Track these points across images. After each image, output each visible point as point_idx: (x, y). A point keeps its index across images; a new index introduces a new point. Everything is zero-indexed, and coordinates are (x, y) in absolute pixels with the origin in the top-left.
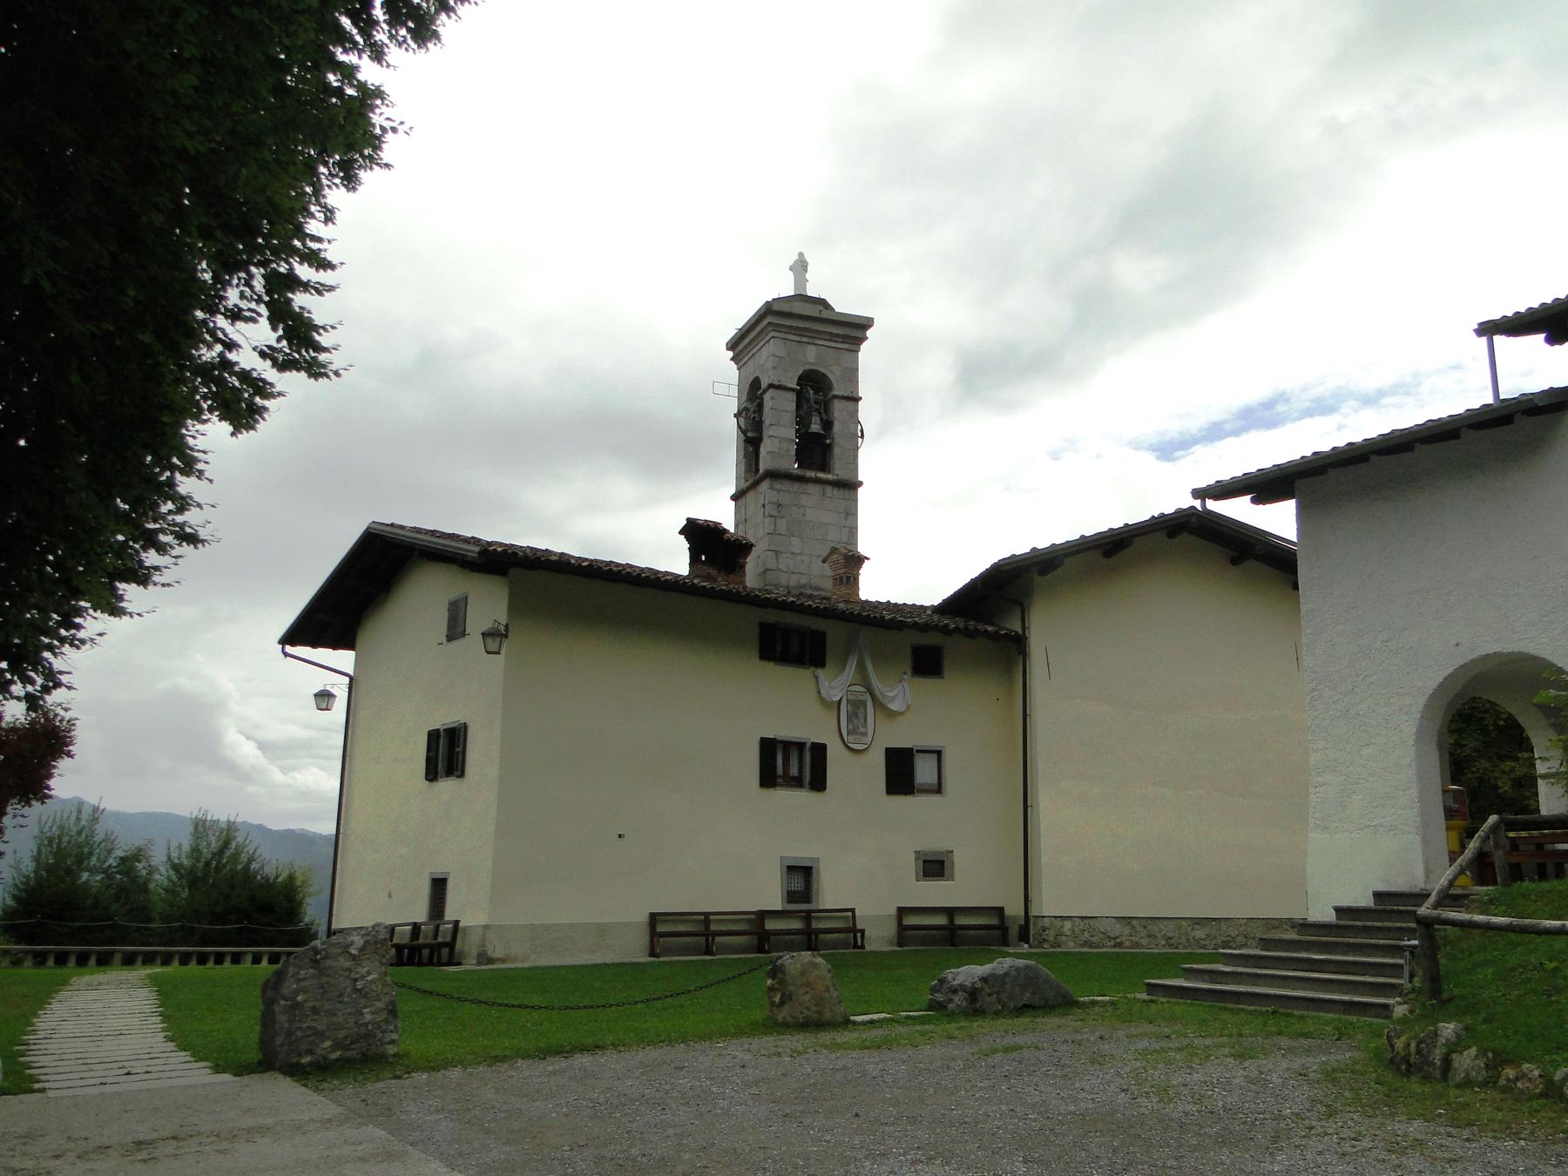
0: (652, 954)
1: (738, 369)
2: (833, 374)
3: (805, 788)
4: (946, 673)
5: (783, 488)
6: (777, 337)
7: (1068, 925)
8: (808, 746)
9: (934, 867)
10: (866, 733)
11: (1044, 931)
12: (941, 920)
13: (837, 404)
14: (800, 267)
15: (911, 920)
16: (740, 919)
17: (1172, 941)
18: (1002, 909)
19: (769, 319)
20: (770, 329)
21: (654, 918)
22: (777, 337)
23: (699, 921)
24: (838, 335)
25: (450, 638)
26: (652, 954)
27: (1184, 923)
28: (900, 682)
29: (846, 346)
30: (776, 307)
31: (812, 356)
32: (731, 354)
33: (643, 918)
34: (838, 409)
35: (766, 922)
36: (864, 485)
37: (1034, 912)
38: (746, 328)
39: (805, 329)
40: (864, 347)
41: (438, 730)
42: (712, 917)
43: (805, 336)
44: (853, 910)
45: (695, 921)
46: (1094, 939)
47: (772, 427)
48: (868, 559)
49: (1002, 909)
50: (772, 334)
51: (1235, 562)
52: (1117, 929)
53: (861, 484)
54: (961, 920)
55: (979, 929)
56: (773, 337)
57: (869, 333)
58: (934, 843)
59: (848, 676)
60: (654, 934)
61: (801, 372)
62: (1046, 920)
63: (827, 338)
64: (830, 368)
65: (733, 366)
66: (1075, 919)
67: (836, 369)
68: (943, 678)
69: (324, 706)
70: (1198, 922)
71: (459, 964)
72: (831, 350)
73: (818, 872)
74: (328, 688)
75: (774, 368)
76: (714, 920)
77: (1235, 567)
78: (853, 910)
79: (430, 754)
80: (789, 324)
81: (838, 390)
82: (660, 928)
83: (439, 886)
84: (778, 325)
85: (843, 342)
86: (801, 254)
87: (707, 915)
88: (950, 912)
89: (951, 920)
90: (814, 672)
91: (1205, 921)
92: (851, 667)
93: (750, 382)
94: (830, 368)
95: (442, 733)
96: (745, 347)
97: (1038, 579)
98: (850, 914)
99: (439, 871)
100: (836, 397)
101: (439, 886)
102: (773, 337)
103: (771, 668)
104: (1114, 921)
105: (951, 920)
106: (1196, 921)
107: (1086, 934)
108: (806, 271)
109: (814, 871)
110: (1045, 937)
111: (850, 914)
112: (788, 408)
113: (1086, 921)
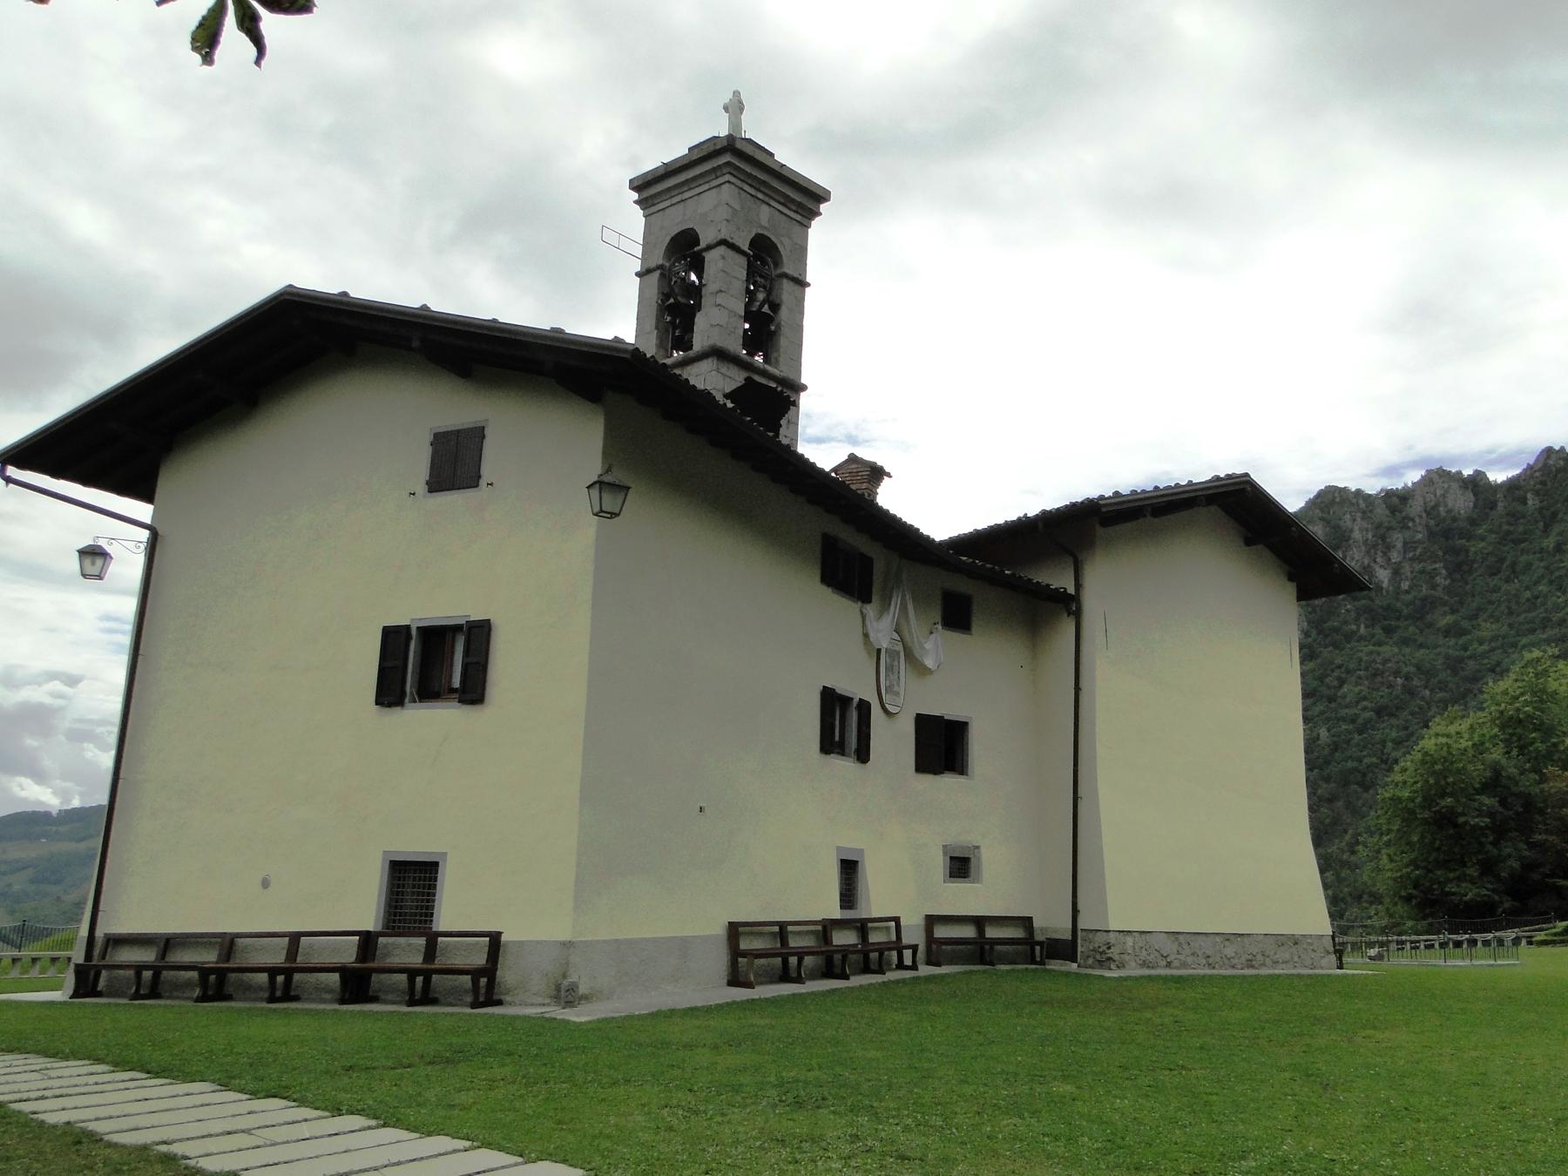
0: (735, 980)
1: (645, 216)
2: (784, 248)
3: (849, 756)
4: (974, 628)
5: (728, 373)
6: (733, 183)
7: (1129, 941)
8: (856, 701)
9: (960, 867)
10: (899, 693)
11: (1109, 948)
12: (969, 932)
13: (786, 285)
14: (735, 107)
15: (941, 932)
16: (808, 931)
17: (1211, 960)
18: (1030, 919)
19: (727, 158)
20: (725, 170)
21: (735, 931)
22: (733, 183)
23: (772, 934)
24: (793, 201)
25: (438, 483)
26: (735, 980)
27: (1218, 939)
28: (931, 633)
29: (798, 217)
30: (739, 145)
31: (766, 217)
32: (635, 196)
33: (719, 929)
34: (786, 290)
35: (935, 931)
36: (808, 390)
37: (1083, 924)
38: (673, 167)
39: (764, 183)
40: (816, 224)
41: (408, 628)
42: (790, 928)
43: (761, 192)
44: (897, 920)
45: (808, 932)
46: (1150, 958)
47: (719, 294)
48: (889, 475)
49: (1030, 919)
50: (727, 177)
51: (1248, 542)
52: (1169, 947)
53: (804, 388)
54: (992, 933)
55: (1018, 944)
56: (729, 182)
57: (823, 207)
58: (961, 835)
59: (895, 612)
60: (735, 953)
61: (753, 235)
62: (1111, 935)
63: (782, 201)
64: (782, 239)
65: (638, 212)
66: (1135, 934)
67: (786, 241)
68: (971, 634)
69: (95, 570)
70: (1228, 938)
71: (499, 1003)
72: (784, 217)
73: (979, 867)
74: (102, 543)
75: (727, 220)
76: (791, 932)
77: (1247, 548)
78: (897, 920)
79: (469, 660)
80: (749, 171)
81: (788, 268)
82: (744, 945)
83: (849, 869)
84: (738, 168)
85: (795, 212)
86: (736, 94)
87: (783, 926)
88: (979, 922)
89: (981, 931)
90: (862, 607)
91: (1232, 938)
92: (896, 607)
93: (673, 235)
94: (782, 239)
95: (414, 632)
96: (669, 189)
97: (1100, 531)
98: (893, 923)
99: (414, 847)
100: (785, 276)
101: (849, 869)
102: (729, 182)
103: (827, 592)
104: (1165, 935)
105: (981, 931)
106: (1227, 937)
107: (1144, 953)
108: (742, 113)
109: (860, 863)
110: (1111, 955)
111: (893, 923)
112: (740, 276)
113: (1143, 936)
